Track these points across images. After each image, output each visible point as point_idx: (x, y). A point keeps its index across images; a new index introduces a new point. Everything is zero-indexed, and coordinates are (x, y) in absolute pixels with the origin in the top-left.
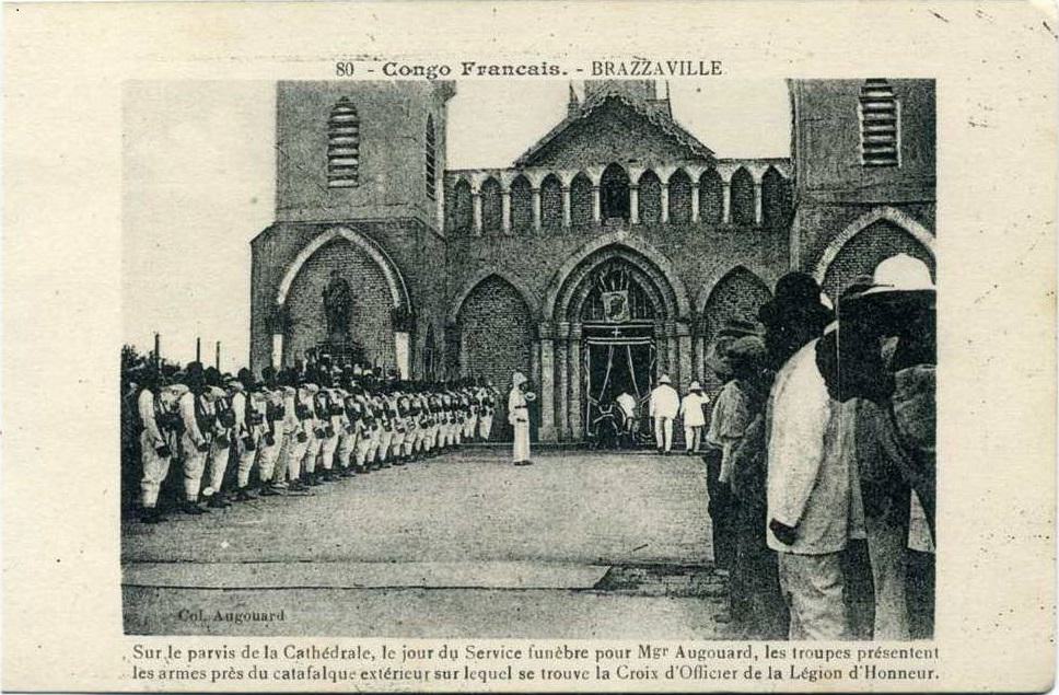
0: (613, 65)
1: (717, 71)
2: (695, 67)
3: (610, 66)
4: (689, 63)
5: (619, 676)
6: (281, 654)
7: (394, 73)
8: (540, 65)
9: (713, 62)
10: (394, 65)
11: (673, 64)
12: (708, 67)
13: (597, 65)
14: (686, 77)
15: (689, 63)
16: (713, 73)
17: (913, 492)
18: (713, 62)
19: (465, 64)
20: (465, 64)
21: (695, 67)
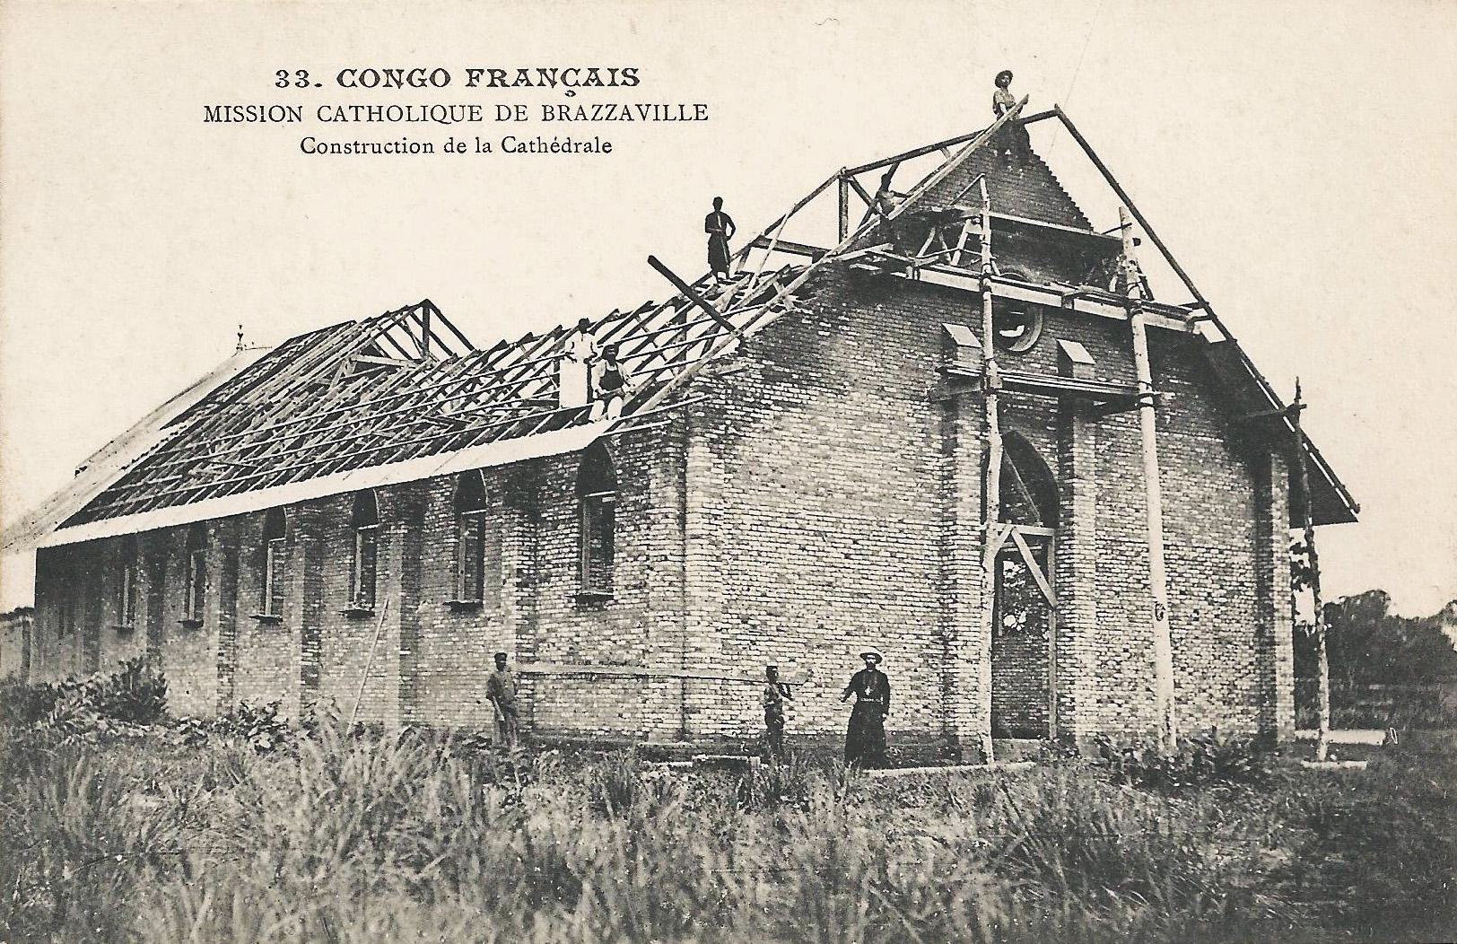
0: (568, 109)
1: (701, 116)
2: (674, 112)
3: (564, 109)
4: (666, 106)
5: (446, 73)
6: (496, 147)
7: (353, 84)
8: (401, 142)
9: (697, 106)
10: (353, 72)
11: (644, 109)
12: (690, 112)
13: (549, 109)
14: (661, 123)
15: (666, 106)
16: (697, 119)
17: (1371, 687)
18: (697, 106)
19: (470, 71)
20: (470, 71)
21: (674, 112)
